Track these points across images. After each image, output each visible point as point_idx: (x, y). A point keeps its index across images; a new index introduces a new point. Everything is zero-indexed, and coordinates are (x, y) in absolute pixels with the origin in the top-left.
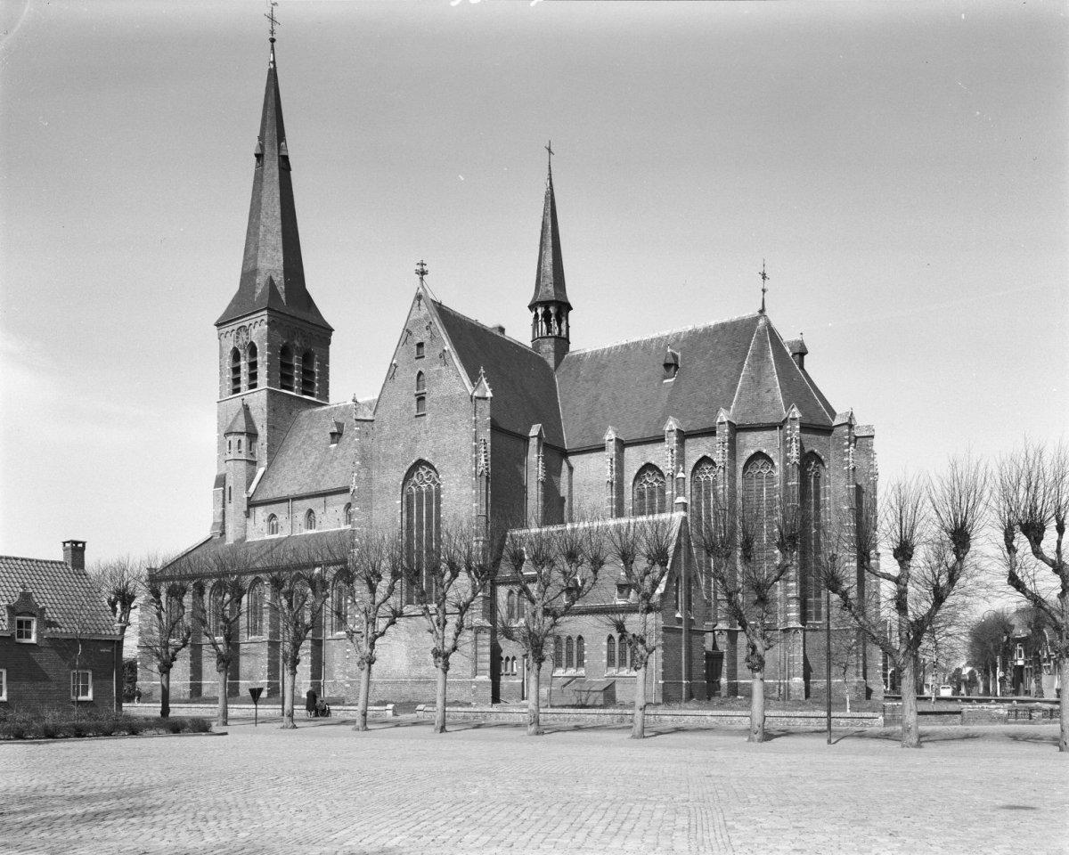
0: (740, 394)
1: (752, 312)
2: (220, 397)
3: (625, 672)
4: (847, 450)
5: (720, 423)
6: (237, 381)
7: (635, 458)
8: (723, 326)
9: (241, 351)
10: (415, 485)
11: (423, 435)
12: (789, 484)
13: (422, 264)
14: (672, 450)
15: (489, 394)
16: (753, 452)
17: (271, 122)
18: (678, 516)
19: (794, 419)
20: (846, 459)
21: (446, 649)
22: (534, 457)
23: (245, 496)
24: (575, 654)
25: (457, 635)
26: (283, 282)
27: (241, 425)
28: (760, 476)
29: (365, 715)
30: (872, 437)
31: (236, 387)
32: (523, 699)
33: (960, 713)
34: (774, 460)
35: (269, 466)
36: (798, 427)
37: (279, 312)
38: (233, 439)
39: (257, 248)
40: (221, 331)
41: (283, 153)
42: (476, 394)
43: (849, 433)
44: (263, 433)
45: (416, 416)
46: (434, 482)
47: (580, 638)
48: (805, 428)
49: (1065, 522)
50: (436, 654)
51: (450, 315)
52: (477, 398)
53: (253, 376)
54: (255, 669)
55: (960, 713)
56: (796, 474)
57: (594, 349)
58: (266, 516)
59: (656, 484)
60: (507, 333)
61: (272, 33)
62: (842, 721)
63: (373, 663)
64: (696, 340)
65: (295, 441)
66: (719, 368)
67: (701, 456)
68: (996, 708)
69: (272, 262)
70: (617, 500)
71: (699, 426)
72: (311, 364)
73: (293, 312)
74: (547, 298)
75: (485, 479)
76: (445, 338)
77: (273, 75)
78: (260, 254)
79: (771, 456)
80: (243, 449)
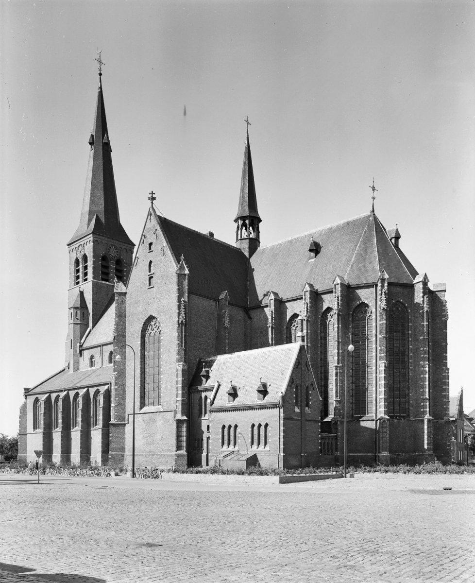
8: (348, 223)
9: (80, 260)
30: (445, 291)
41: (105, 141)
53: (86, 274)
60: (215, 237)
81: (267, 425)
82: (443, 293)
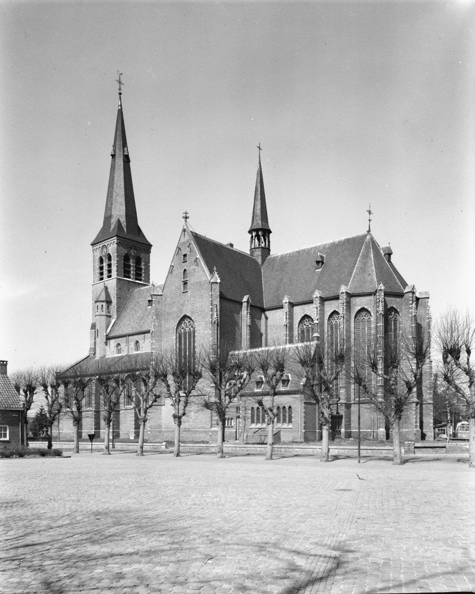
0: (354, 277)
1: (363, 232)
2: (94, 283)
3: (285, 426)
4: (411, 306)
5: (342, 293)
6: (102, 274)
7: (299, 312)
8: (348, 240)
9: (104, 258)
10: (183, 328)
11: (186, 302)
12: (378, 325)
13: (186, 213)
14: (317, 308)
15: (219, 281)
16: (360, 308)
17: (119, 138)
18: (314, 343)
19: (381, 290)
20: (411, 311)
21: (180, 414)
22: (245, 312)
23: (105, 334)
24: (261, 417)
25: (185, 407)
26: (125, 221)
27: (103, 297)
28: (364, 320)
29: (142, 448)
31: (102, 277)
32: (236, 439)
33: (445, 447)
34: (371, 312)
35: (117, 318)
36: (383, 294)
37: (122, 237)
38: (99, 304)
39: (112, 204)
40: (94, 248)
41: (126, 153)
42: (212, 281)
43: (412, 297)
44: (114, 301)
45: (183, 293)
46: (192, 327)
47: (290, 407)
48: (387, 294)
49: (470, 349)
50: (175, 416)
51: (201, 239)
52: (212, 283)
53: (110, 271)
54: (88, 427)
55: (445, 447)
56: (382, 320)
57: (282, 254)
58: (115, 344)
59: (310, 326)
61: (120, 90)
62: (384, 451)
63: (146, 421)
64: (334, 248)
65: (131, 305)
66: (345, 263)
67: (332, 310)
68: (465, 445)
69: (119, 212)
70: (289, 335)
71: (332, 295)
72: (140, 264)
73: (130, 237)
74: (258, 227)
75: (216, 325)
76: (197, 252)
77: (120, 113)
78: (113, 207)
79: (369, 310)
80: (104, 309)
81: (290, 407)
82: (427, 300)
